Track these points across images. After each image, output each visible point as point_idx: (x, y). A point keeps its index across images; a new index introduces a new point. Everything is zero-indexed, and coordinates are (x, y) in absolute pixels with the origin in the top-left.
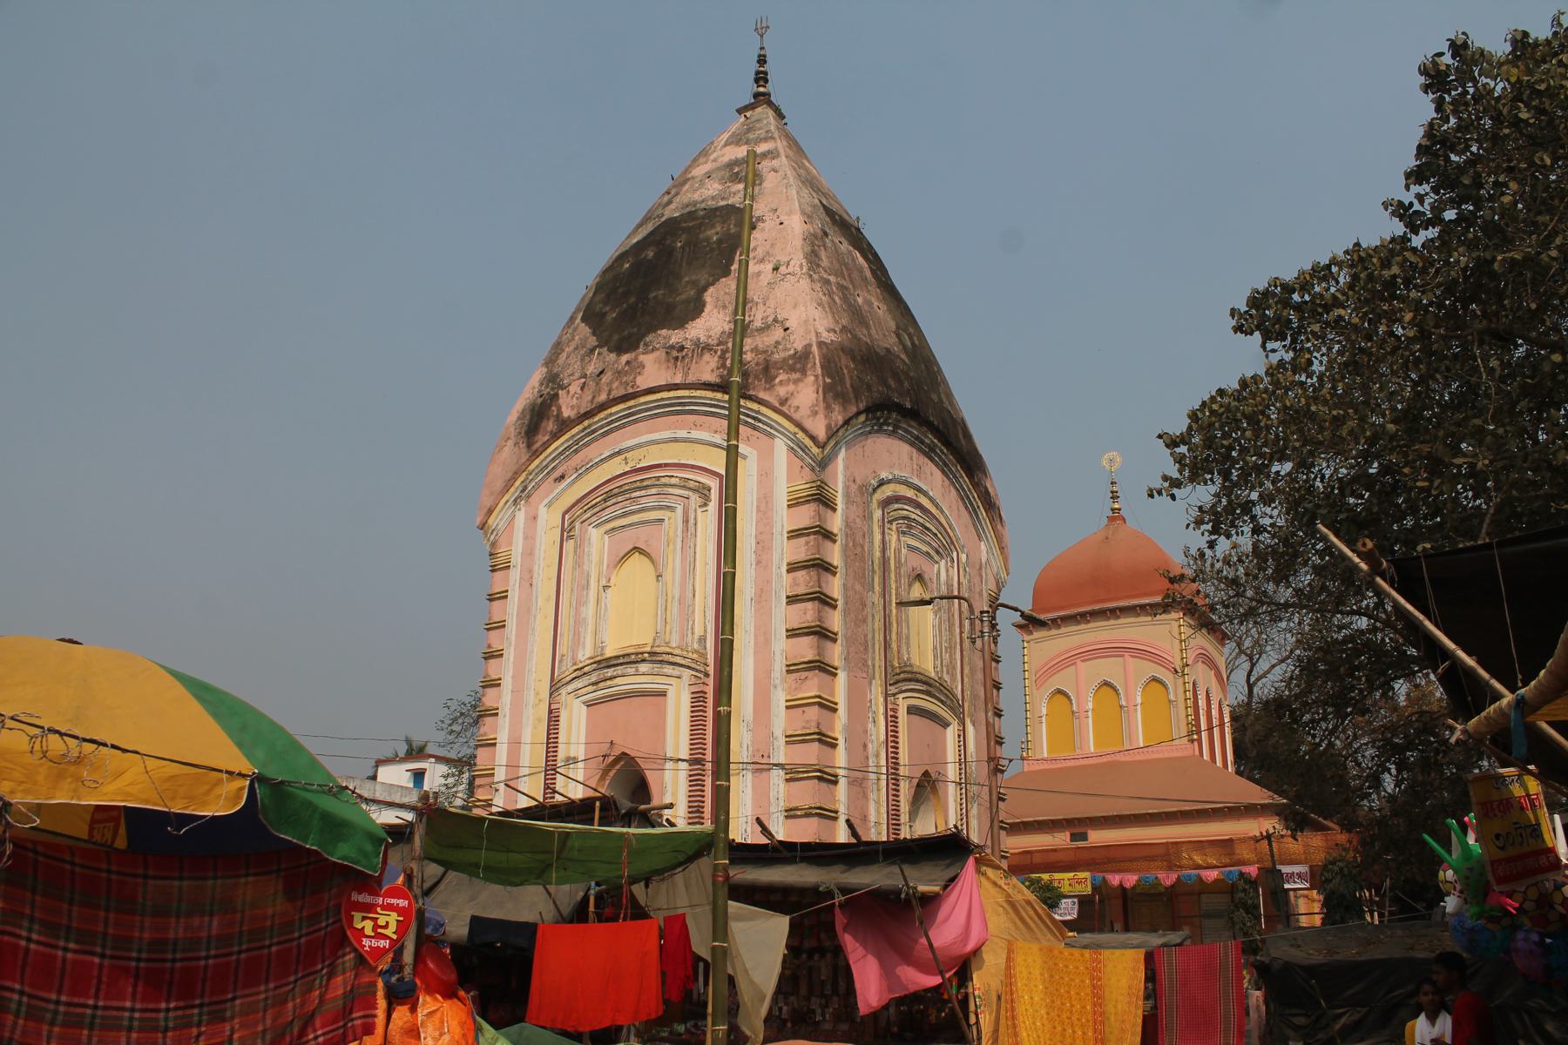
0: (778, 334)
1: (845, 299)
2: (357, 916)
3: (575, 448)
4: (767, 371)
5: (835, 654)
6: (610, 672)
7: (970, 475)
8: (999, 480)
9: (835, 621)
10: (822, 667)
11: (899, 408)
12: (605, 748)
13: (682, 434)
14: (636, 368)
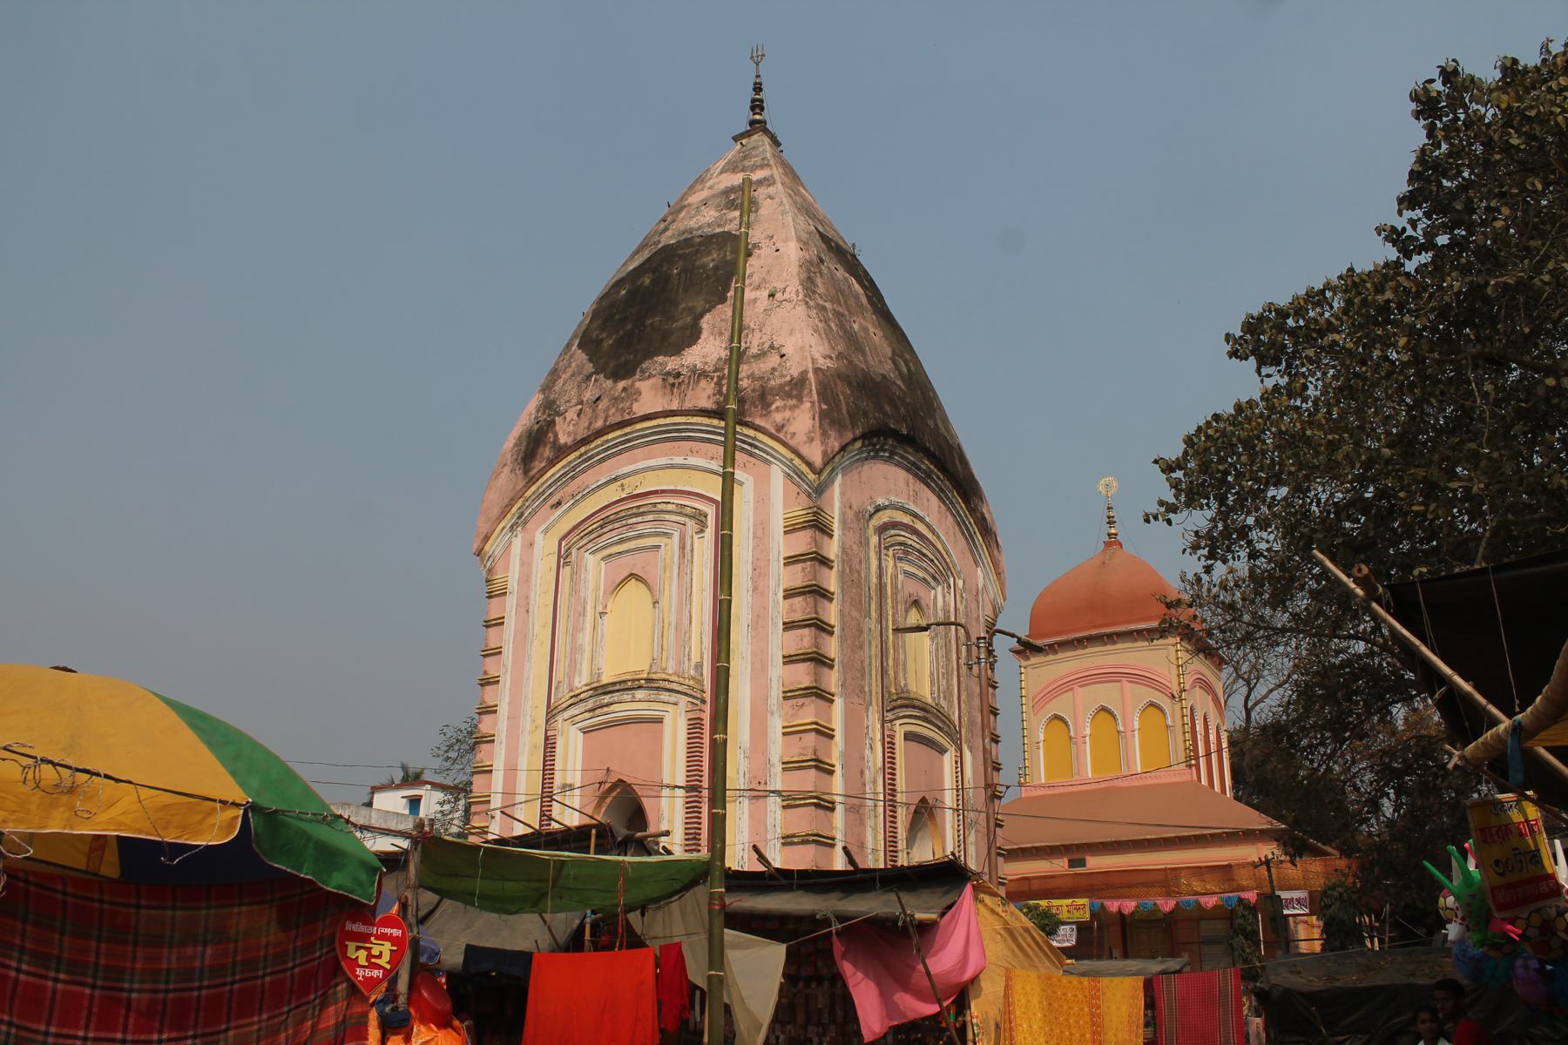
0: (774, 360)
1: (841, 326)
2: (351, 945)
3: (572, 474)
4: (764, 398)
5: (832, 680)
6: (607, 699)
9: (832, 647)
10: (819, 693)
11: (896, 435)
12: (601, 775)
13: (678, 460)
14: (632, 394)
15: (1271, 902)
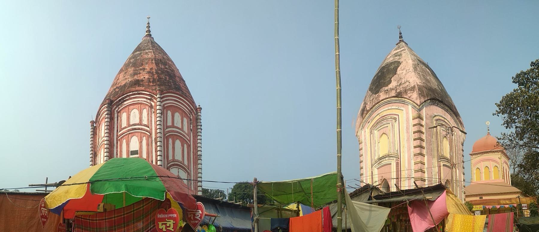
0: (408, 83)
1: (424, 77)
2: (160, 223)
3: (370, 116)
4: (406, 91)
5: (424, 152)
6: (381, 161)
7: (456, 116)
8: (463, 119)
9: (424, 144)
10: (421, 154)
11: (438, 100)
12: (381, 178)
13: (390, 108)
14: (379, 96)
15: (520, 205)
